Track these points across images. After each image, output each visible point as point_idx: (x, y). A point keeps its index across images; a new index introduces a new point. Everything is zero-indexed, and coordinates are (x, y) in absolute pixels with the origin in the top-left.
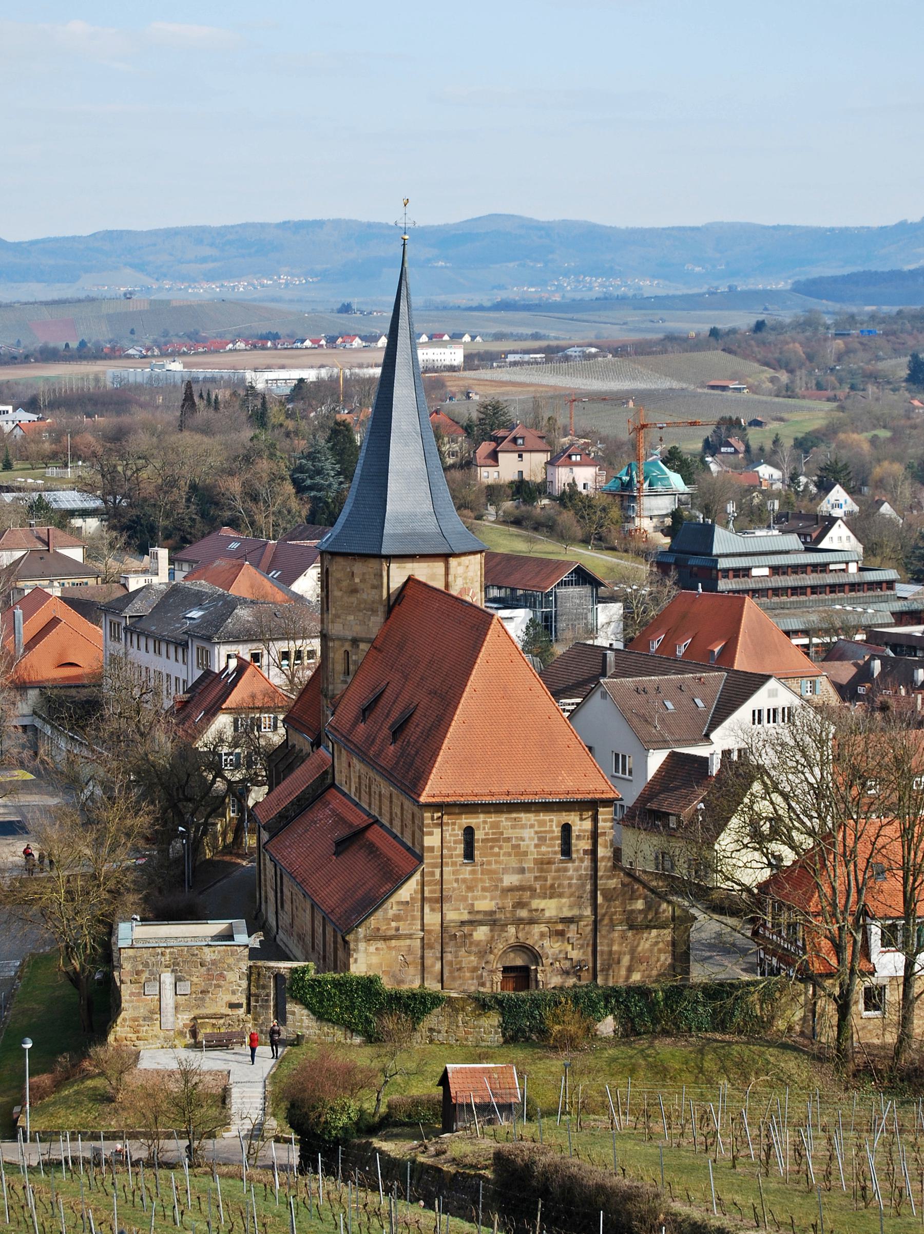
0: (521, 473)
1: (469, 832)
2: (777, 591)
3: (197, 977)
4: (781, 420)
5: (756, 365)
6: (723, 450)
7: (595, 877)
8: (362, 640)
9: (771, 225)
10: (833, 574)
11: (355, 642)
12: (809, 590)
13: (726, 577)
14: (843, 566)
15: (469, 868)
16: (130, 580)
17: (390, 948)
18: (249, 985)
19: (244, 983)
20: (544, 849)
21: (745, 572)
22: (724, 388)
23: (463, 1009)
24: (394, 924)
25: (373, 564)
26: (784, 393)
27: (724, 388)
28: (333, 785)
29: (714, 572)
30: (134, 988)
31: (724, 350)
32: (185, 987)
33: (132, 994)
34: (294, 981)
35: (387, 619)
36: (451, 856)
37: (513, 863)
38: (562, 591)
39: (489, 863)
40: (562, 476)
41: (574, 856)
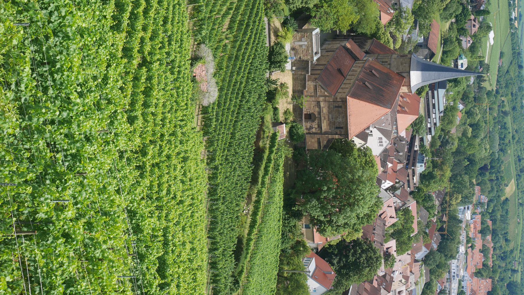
11: (390, 64)
21: (433, 97)
28: (356, 60)
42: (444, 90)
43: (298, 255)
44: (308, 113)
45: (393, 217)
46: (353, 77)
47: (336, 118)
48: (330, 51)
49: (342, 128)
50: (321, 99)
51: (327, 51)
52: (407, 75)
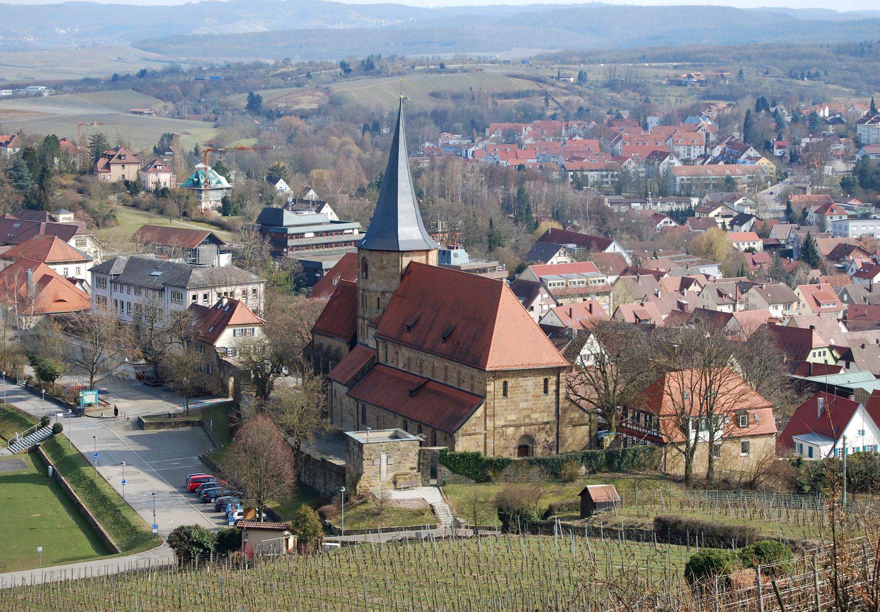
0: (123, 176)
1: (505, 383)
2: (317, 246)
3: (396, 456)
4: (187, 134)
5: (153, 98)
6: (166, 153)
7: (557, 402)
8: (387, 292)
9: (106, 4)
10: (346, 235)
11: (383, 293)
12: (334, 245)
13: (292, 238)
14: (351, 231)
15: (505, 400)
17: (472, 439)
18: (419, 458)
19: (417, 458)
20: (536, 390)
21: (301, 235)
22: (141, 113)
23: (521, 465)
24: (473, 428)
25: (395, 255)
26: (176, 116)
27: (141, 113)
28: (378, 363)
29: (285, 235)
30: (369, 462)
31: (133, 89)
32: (391, 461)
33: (368, 465)
34: (442, 456)
35: (401, 281)
36: (498, 395)
37: (524, 397)
38: (201, 248)
39: (514, 398)
40: (151, 179)
42: (285, 211)
44: (517, 451)
46: (425, 364)
47: (526, 392)
48: (364, 416)
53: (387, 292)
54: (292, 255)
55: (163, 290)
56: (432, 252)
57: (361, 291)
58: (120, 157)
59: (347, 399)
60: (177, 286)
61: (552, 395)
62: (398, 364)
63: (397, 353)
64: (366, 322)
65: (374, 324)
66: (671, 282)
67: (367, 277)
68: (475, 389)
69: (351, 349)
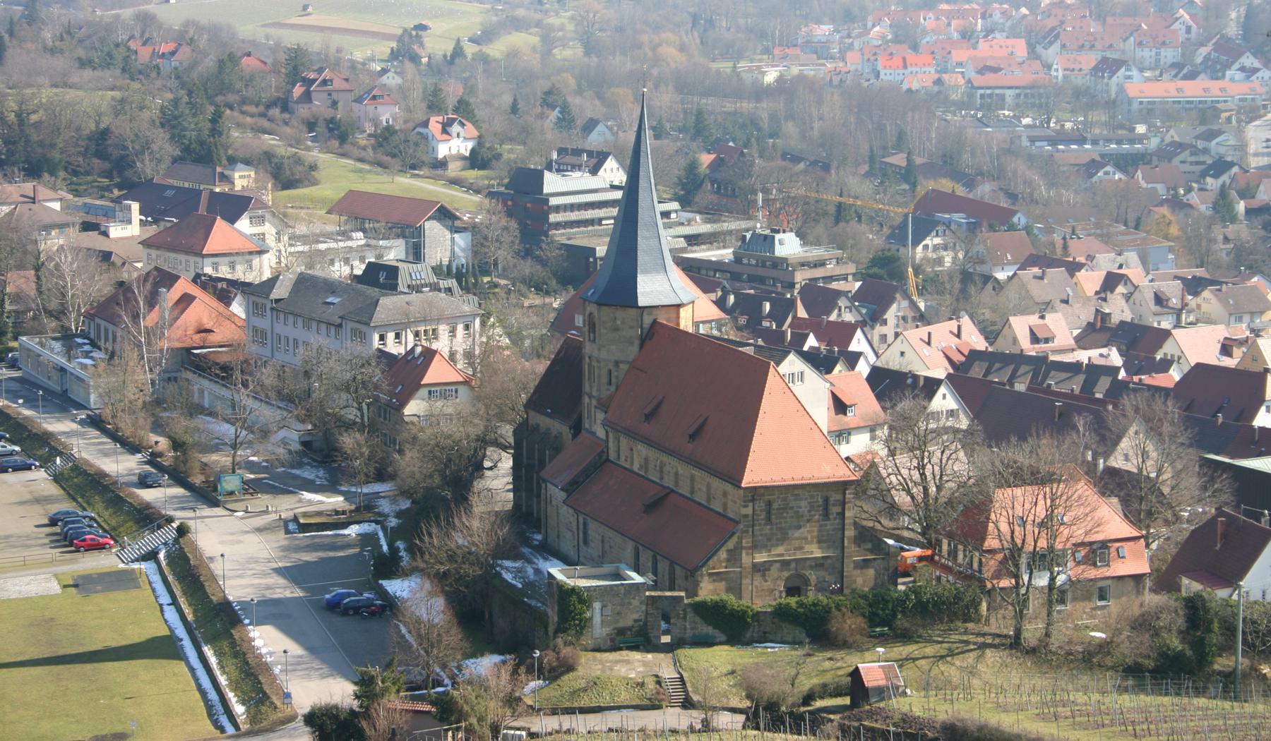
8: (623, 362)
11: (617, 363)
16: (111, 229)
28: (608, 460)
38: (428, 225)
41: (831, 517)
42: (547, 175)
43: (115, 513)
45: (959, 327)
46: (667, 468)
48: (585, 533)
49: (826, 500)
50: (746, 559)
51: (586, 542)
52: (650, 314)
53: (623, 362)
54: (560, 236)
55: (340, 326)
56: (686, 308)
57: (587, 359)
58: (325, 82)
59: (565, 507)
60: (358, 322)
61: (835, 519)
62: (632, 464)
63: (632, 450)
64: (594, 402)
65: (604, 405)
66: (1090, 280)
67: (594, 340)
68: (729, 510)
69: (575, 436)
